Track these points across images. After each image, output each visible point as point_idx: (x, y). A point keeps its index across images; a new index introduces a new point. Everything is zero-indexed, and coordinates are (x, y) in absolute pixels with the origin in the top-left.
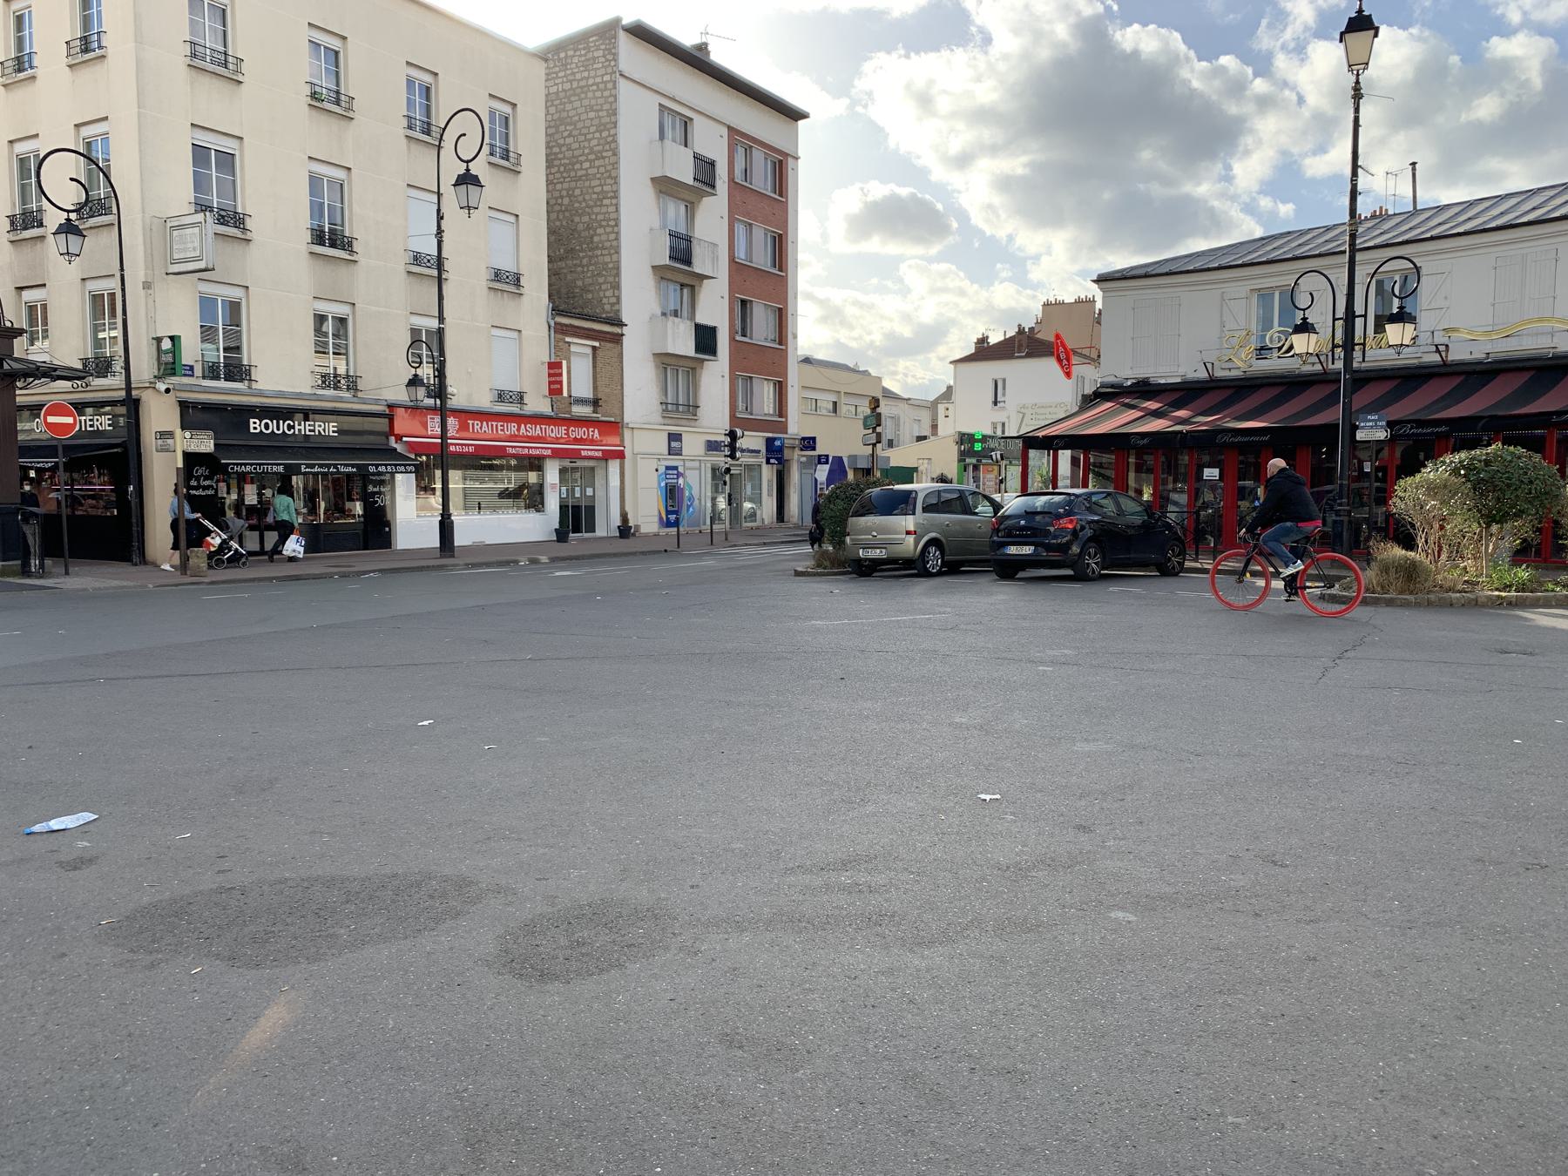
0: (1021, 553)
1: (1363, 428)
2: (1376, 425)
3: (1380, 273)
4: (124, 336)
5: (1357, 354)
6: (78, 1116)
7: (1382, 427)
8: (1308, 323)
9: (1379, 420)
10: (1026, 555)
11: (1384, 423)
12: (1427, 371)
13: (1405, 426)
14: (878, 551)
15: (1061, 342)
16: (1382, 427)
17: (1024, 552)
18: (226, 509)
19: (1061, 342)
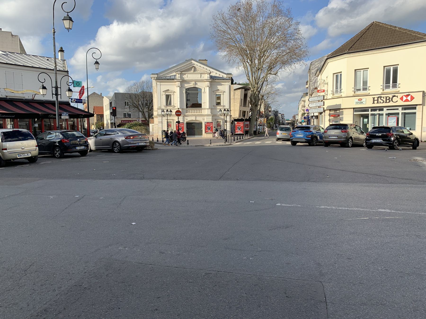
0: (81, 149)
1: (63, 115)
2: (66, 115)
3: (68, 78)
4: (399, 122)
5: (59, 96)
6: (313, 264)
7: (67, 116)
8: (70, 89)
9: (67, 114)
10: (83, 149)
11: (68, 115)
12: (27, 101)
13: (51, 115)
14: (26, 154)
15: (83, 89)
16: (67, 116)
17: (82, 148)
18: (14, 161)
19: (83, 89)
